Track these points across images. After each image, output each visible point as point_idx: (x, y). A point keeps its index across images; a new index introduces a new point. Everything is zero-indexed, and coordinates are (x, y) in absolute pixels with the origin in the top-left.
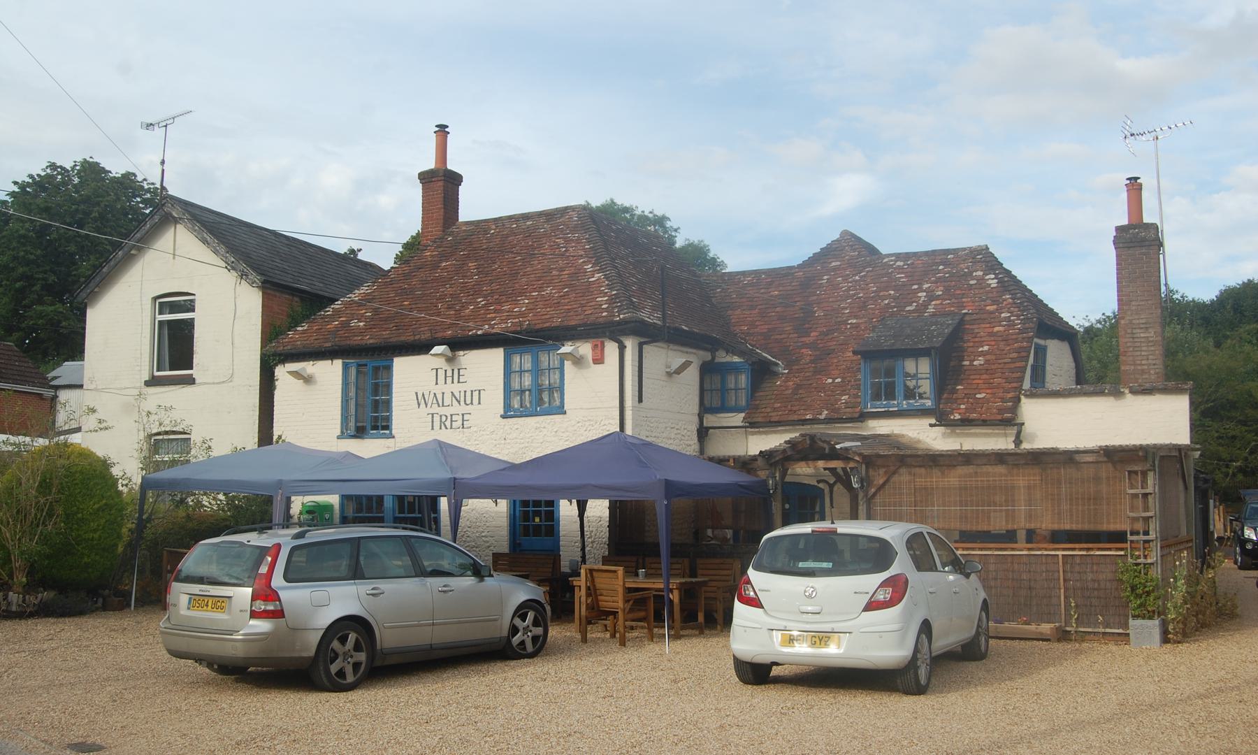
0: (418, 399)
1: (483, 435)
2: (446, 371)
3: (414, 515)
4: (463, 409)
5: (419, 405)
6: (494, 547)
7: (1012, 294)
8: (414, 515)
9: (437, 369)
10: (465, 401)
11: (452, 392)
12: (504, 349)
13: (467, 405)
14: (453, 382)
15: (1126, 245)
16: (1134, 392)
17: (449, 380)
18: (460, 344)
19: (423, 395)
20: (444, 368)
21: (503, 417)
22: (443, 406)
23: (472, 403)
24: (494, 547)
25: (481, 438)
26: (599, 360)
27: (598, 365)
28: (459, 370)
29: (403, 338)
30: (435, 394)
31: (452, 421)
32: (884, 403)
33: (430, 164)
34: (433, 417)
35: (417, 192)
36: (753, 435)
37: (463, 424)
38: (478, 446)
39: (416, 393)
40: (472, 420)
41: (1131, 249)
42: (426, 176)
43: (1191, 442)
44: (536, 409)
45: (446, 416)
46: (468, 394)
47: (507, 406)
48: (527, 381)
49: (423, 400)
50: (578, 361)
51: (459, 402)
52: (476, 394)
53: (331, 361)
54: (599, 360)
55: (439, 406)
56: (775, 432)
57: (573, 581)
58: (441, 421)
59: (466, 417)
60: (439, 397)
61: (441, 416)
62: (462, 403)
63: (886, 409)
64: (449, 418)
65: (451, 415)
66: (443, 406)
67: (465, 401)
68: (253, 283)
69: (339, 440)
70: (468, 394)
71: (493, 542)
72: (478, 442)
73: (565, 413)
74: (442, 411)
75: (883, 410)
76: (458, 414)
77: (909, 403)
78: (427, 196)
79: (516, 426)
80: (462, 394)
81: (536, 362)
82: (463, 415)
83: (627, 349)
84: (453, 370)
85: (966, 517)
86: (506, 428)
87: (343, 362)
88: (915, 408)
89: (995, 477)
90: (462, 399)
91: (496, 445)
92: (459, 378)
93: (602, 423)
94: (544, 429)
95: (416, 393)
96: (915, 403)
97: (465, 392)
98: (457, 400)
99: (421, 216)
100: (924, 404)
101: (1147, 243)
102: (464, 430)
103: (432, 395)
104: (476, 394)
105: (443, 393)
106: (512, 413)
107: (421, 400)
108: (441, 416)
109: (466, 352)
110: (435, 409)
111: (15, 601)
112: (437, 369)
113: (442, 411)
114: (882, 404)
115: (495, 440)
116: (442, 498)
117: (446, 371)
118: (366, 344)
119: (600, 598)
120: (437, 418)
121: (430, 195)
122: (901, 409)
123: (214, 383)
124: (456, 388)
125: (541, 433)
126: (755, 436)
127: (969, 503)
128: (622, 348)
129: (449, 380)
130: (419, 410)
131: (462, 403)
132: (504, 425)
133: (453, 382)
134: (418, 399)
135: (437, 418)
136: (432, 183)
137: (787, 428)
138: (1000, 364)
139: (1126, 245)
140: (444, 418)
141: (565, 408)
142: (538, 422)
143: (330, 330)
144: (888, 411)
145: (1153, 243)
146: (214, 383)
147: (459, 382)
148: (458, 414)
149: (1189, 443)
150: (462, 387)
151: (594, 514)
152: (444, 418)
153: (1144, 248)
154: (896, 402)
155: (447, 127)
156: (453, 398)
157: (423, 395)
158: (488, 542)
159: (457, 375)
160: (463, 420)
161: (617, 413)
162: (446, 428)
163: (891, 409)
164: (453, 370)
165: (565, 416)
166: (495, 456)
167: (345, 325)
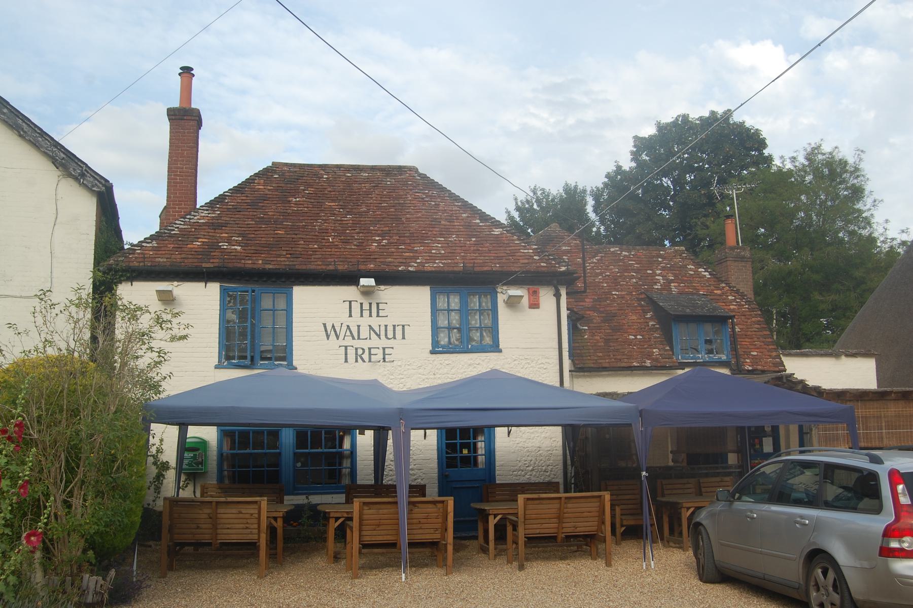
0: (326, 331)
1: (408, 369)
2: (361, 304)
3: (319, 450)
4: (384, 342)
5: (328, 337)
6: (422, 479)
7: (726, 284)
8: (319, 450)
9: (350, 302)
10: (386, 335)
11: (370, 326)
12: (430, 287)
13: (390, 339)
14: (371, 316)
15: (733, 259)
16: (847, 356)
17: (366, 313)
18: (386, 278)
19: (333, 326)
20: (360, 301)
21: (432, 352)
22: (359, 338)
23: (394, 338)
24: (422, 479)
25: (405, 373)
26: (534, 305)
27: (533, 310)
28: (378, 304)
29: (313, 267)
30: (348, 326)
31: (370, 354)
32: (691, 356)
33: (176, 104)
34: (346, 349)
35: (165, 126)
36: (578, 378)
37: (384, 359)
38: (403, 380)
39: (325, 325)
40: (394, 354)
41: (737, 262)
42: (177, 113)
43: (878, 387)
44: (468, 346)
45: (363, 349)
46: (390, 329)
47: (435, 343)
48: (455, 318)
49: (333, 332)
50: (512, 303)
51: (379, 336)
52: (399, 330)
53: (204, 284)
54: (534, 305)
55: (354, 338)
56: (599, 376)
57: (683, 503)
58: (356, 354)
59: (387, 351)
60: (354, 330)
61: (356, 349)
62: (383, 336)
63: (694, 361)
64: (367, 351)
65: (370, 349)
66: (359, 338)
67: (386, 335)
68: (93, 186)
69: (217, 370)
70: (390, 329)
71: (421, 474)
72: (402, 377)
73: (500, 351)
74: (357, 343)
75: (692, 361)
76: (378, 348)
77: (709, 357)
78: (176, 132)
79: (447, 362)
80: (383, 328)
81: (464, 304)
82: (384, 349)
83: (562, 297)
84: (370, 304)
85: (867, 439)
86: (435, 362)
87: (220, 285)
88: (714, 360)
89: (870, 409)
90: (383, 333)
91: (424, 380)
92: (378, 312)
93: (540, 362)
94: (478, 366)
95: (325, 325)
96: (714, 356)
97: (386, 326)
98: (376, 333)
99: (168, 151)
100: (721, 358)
101: (745, 260)
102: (386, 363)
103: (344, 328)
104: (399, 330)
105: (359, 326)
106: (441, 349)
107: (330, 331)
108: (356, 349)
109: (388, 287)
110: (349, 341)
111: (92, 586)
112: (350, 302)
113: (357, 343)
114: (690, 356)
115: (423, 375)
116: (497, 429)
117: (361, 304)
118: (236, 267)
119: (219, 531)
120: (351, 352)
121: (179, 132)
122: (705, 360)
123: (21, 297)
124: (375, 322)
125: (475, 369)
126: (580, 379)
127: (890, 427)
128: (558, 296)
129: (366, 313)
130: (328, 341)
131: (383, 336)
132: (433, 361)
133: (371, 316)
134: (326, 331)
135: (351, 352)
136: (183, 121)
137: (610, 372)
138: (751, 331)
139: (733, 259)
140: (360, 351)
141: (500, 347)
142: (472, 359)
143: (419, 245)
144: (696, 362)
145: (749, 260)
146: (21, 297)
147: (378, 316)
148: (378, 348)
149: (876, 388)
150: (383, 322)
151: (533, 444)
152: (360, 351)
153: (743, 262)
154: (700, 356)
155: (192, 69)
156: (332, 329)
157: (333, 326)
158: (414, 475)
159: (378, 310)
160: (384, 354)
161: (557, 353)
162: (364, 361)
163: (698, 361)
164: (370, 304)
165: (500, 354)
166: (550, 384)
167: (213, 246)
